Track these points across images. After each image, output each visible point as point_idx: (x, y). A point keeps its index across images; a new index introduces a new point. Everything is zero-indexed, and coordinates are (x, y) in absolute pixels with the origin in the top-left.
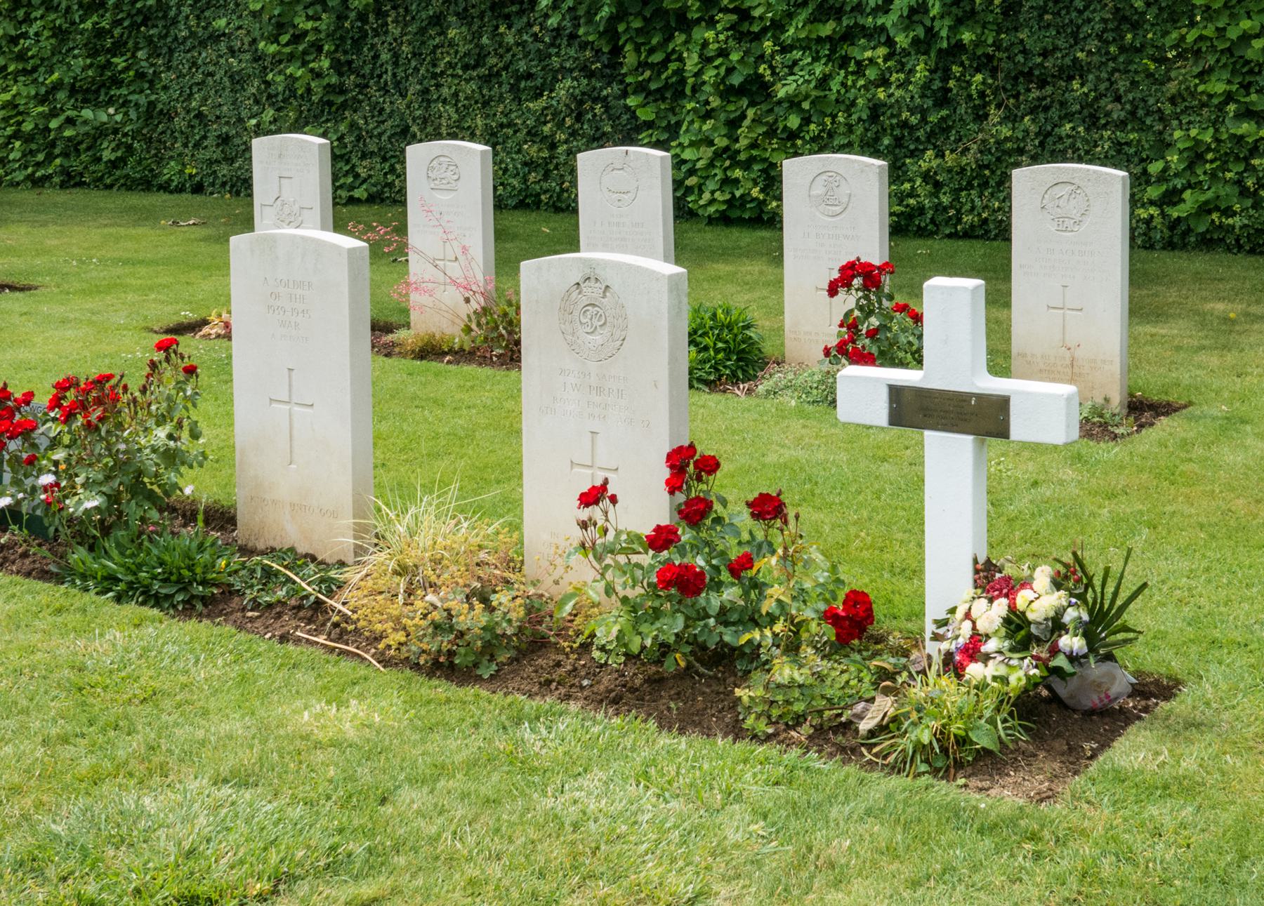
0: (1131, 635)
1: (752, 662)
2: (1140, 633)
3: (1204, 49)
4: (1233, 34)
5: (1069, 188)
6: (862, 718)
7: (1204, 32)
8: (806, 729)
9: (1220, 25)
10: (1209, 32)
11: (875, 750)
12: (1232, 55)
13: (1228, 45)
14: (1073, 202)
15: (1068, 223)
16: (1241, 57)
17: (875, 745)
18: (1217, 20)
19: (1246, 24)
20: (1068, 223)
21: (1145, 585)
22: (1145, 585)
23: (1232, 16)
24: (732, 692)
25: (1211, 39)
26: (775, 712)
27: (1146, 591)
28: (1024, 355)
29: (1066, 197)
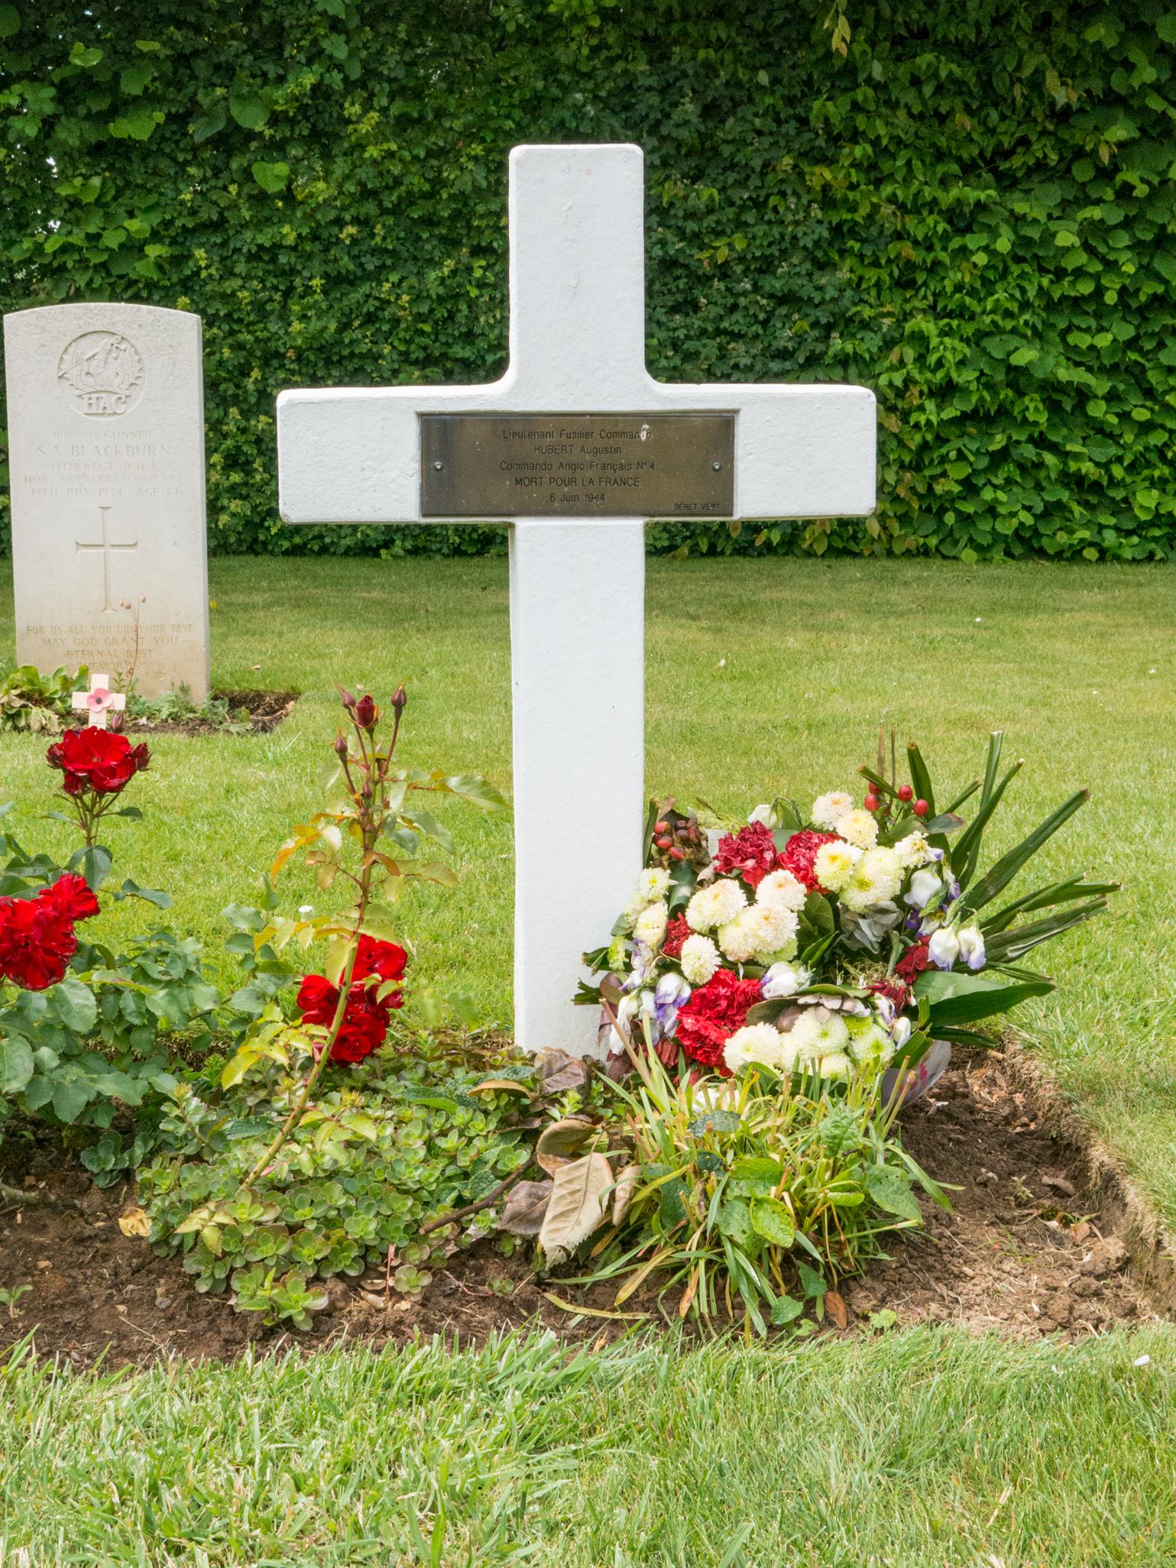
0: (1083, 902)
1: (127, 1146)
2: (1104, 890)
3: (70, 265)
4: (112, 240)
5: (108, 340)
6: (538, 1221)
7: (70, 239)
8: (410, 1280)
9: (92, 229)
10: (77, 238)
11: (624, 1295)
12: (109, 274)
13: (105, 257)
14: (114, 365)
15: (109, 400)
16: (121, 277)
17: (616, 1282)
18: (88, 222)
19: (137, 226)
20: (109, 400)
21: (1082, 797)
22: (1082, 797)
23: (108, 216)
24: (114, 1230)
25: (80, 249)
26: (311, 1251)
27: (1087, 806)
28: (39, 630)
29: (101, 356)
